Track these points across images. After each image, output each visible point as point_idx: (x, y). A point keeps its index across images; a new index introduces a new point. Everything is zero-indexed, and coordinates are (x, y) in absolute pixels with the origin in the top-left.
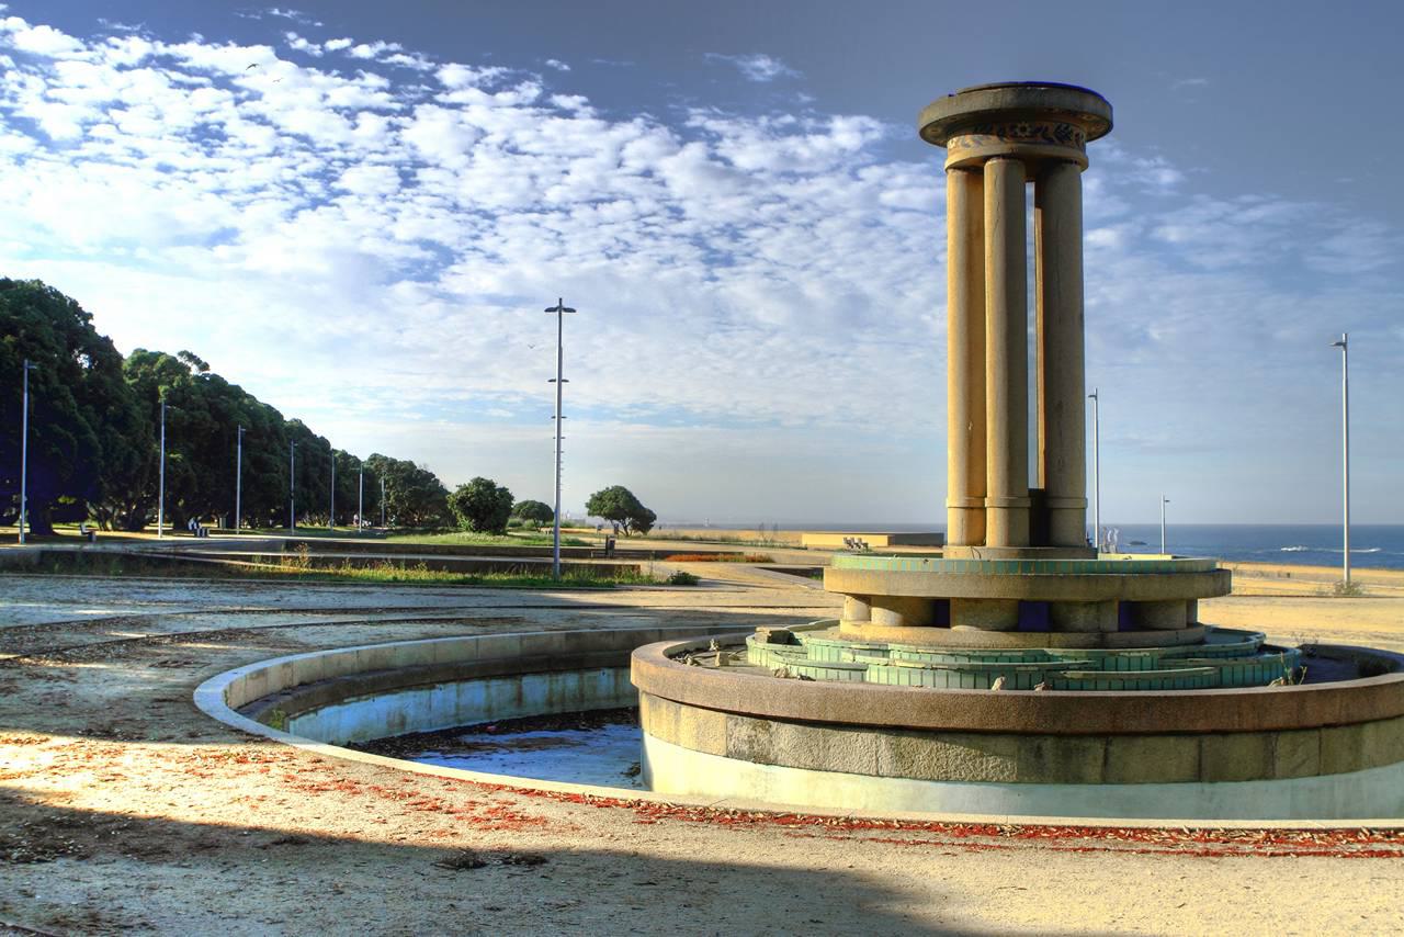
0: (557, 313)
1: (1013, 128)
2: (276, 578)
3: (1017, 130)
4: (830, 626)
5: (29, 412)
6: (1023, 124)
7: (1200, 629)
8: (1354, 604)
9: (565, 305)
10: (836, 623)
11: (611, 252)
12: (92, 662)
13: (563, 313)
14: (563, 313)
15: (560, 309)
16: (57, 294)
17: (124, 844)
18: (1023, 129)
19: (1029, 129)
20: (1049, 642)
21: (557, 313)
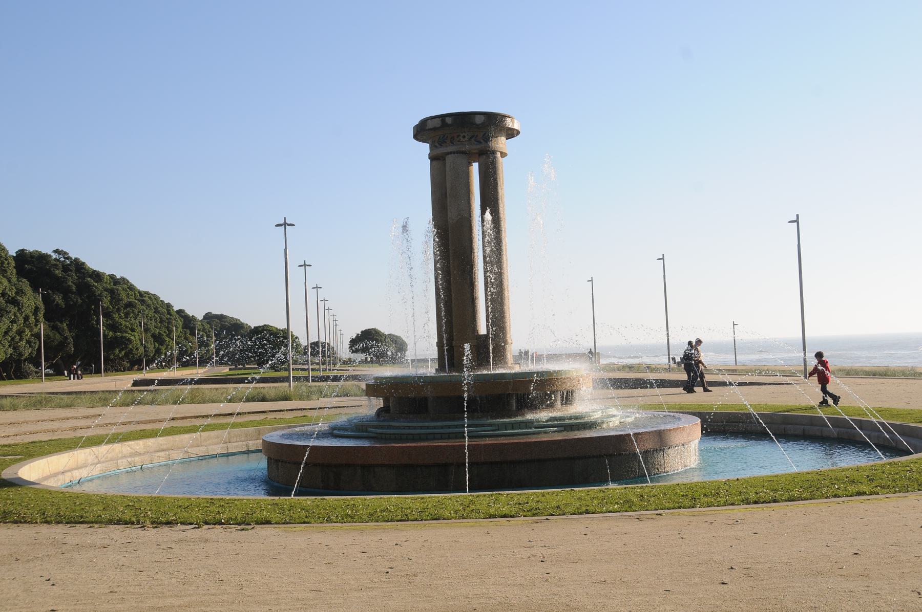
0: (283, 227)
1: (458, 136)
2: (430, 429)
3: (461, 137)
4: (6, 486)
5: (43, 334)
6: (464, 134)
7: (22, 491)
8: (760, 374)
9: (288, 222)
10: (603, 383)
11: (426, 325)
12: (444, 446)
13: (287, 227)
14: (287, 227)
15: (285, 224)
16: (79, 266)
17: (406, 515)
18: (464, 137)
19: (467, 137)
20: (513, 427)
21: (283, 227)
